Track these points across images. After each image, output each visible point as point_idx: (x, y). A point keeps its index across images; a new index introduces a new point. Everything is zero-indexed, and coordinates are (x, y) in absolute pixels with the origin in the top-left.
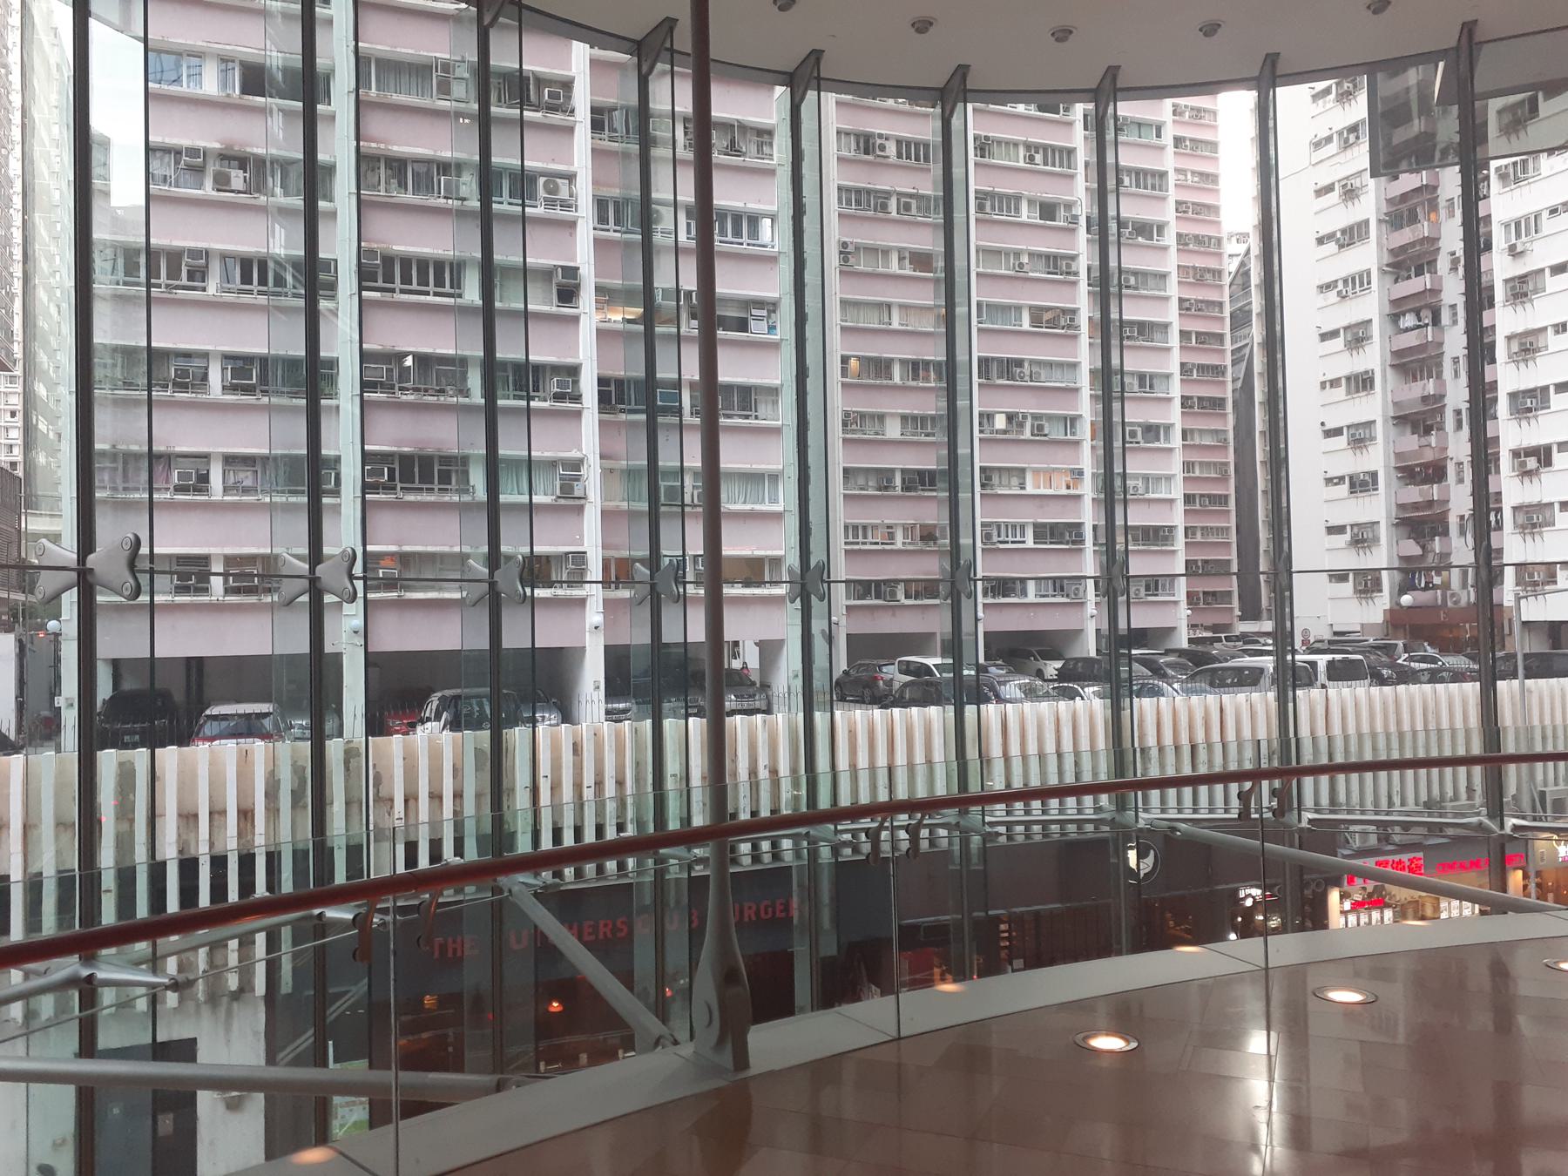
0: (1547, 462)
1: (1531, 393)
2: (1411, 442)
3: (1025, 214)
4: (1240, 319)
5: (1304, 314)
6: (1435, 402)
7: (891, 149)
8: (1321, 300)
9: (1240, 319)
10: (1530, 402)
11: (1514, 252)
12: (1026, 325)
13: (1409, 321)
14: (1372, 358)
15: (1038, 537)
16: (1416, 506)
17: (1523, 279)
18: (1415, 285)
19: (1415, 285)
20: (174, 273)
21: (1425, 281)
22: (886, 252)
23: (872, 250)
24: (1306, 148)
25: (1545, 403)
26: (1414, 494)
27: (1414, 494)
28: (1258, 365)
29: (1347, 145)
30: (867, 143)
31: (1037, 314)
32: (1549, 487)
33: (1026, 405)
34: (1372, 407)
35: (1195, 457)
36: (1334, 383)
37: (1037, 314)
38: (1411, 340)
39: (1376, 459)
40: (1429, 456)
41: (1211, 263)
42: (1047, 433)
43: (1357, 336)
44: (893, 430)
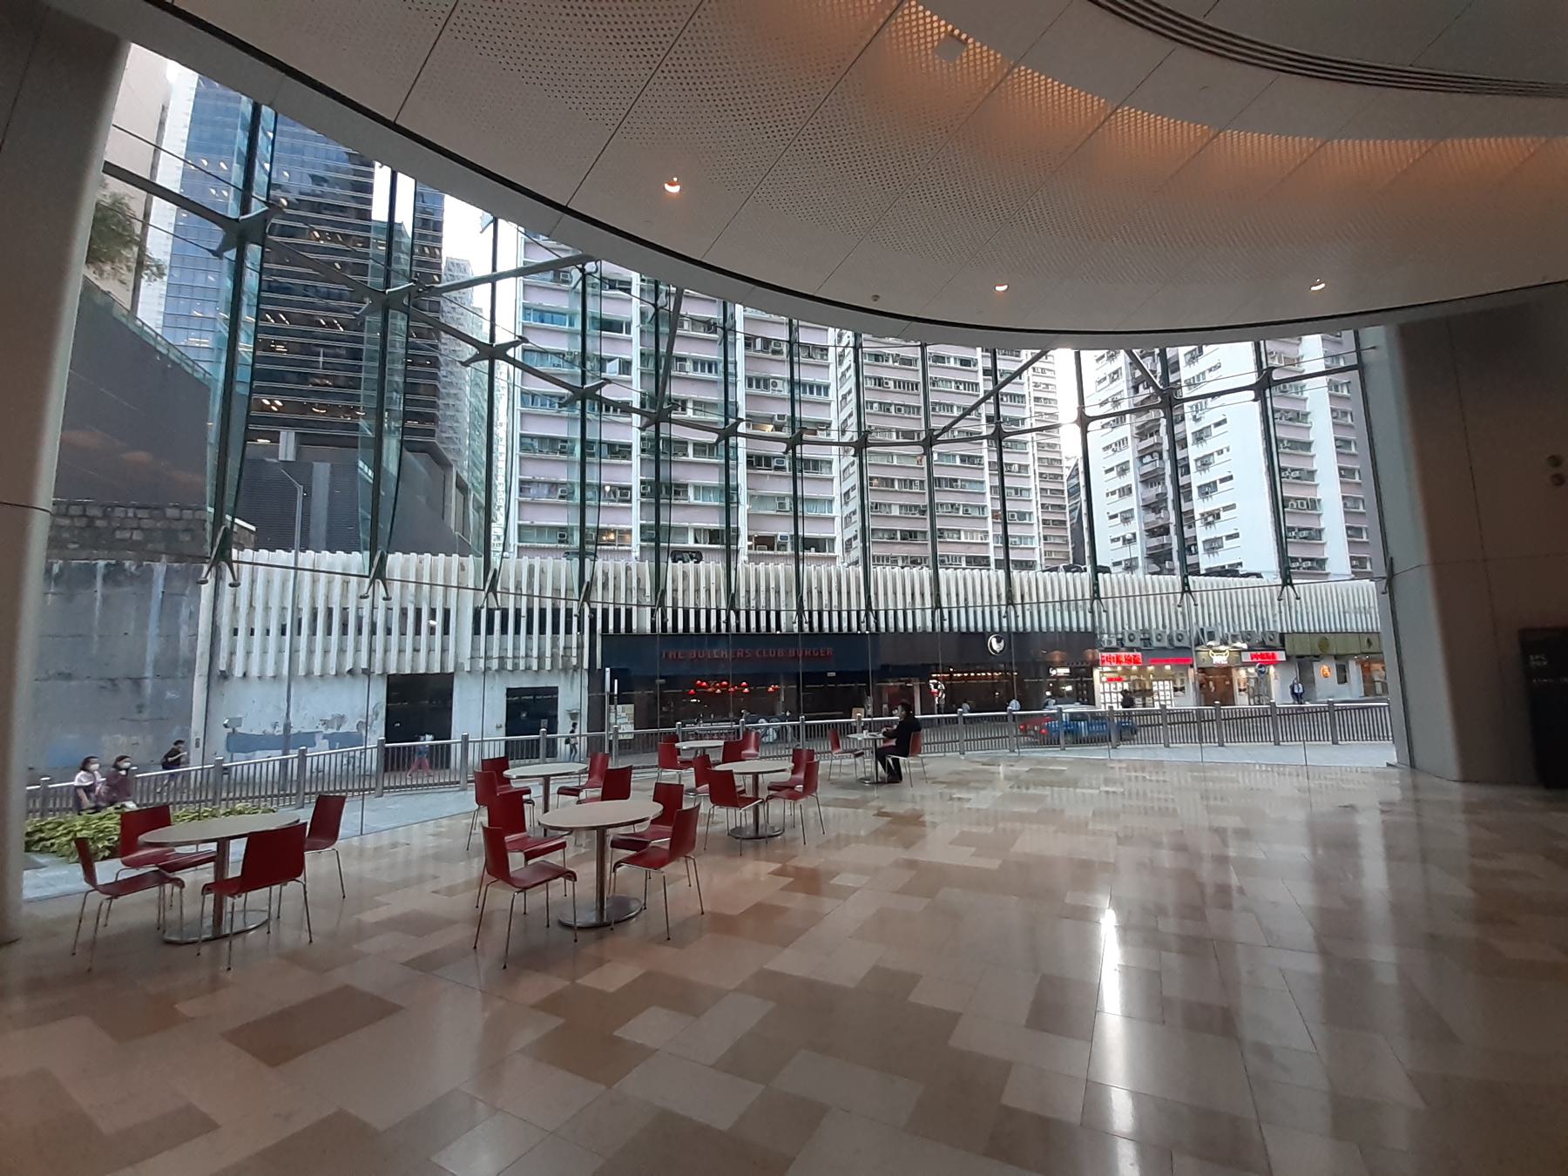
0: (1218, 516)
1: (1208, 485)
2: (1152, 517)
3: (952, 363)
4: (1074, 492)
5: (1102, 484)
6: (1162, 498)
7: (891, 384)
8: (1105, 454)
9: (1074, 492)
10: (1208, 490)
11: (1196, 419)
12: (958, 462)
13: (1148, 459)
14: (1131, 479)
15: (962, 461)
16: (1156, 548)
17: (1201, 431)
18: (1150, 441)
19: (1150, 441)
20: (607, 409)
21: (1154, 439)
22: (890, 431)
23: (884, 430)
24: (1094, 384)
25: (1215, 489)
26: (1154, 542)
27: (1154, 542)
28: (1084, 511)
29: (1113, 380)
30: (879, 381)
31: (963, 458)
32: (1220, 529)
33: (960, 500)
34: (1132, 502)
35: (1049, 548)
36: (1113, 493)
37: (963, 458)
38: (1148, 468)
39: (1135, 526)
40: (1161, 522)
41: (1057, 471)
42: (973, 513)
43: (1123, 469)
44: (896, 511)
